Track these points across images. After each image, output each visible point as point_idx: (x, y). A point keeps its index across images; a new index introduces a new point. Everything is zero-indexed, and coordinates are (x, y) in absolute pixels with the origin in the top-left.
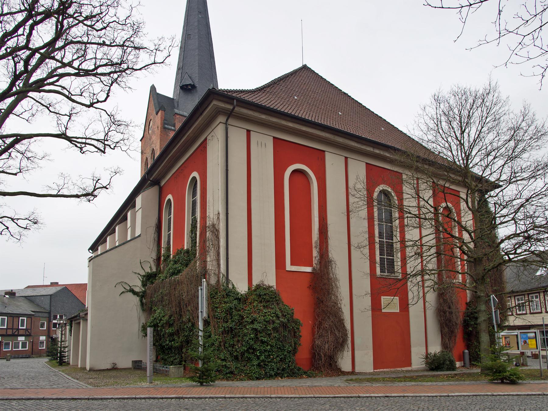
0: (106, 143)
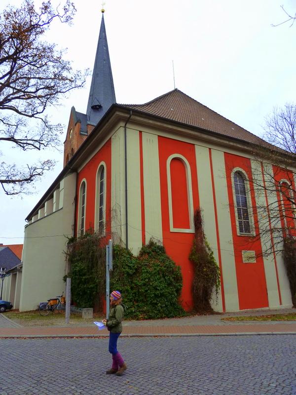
0: (41, 142)
